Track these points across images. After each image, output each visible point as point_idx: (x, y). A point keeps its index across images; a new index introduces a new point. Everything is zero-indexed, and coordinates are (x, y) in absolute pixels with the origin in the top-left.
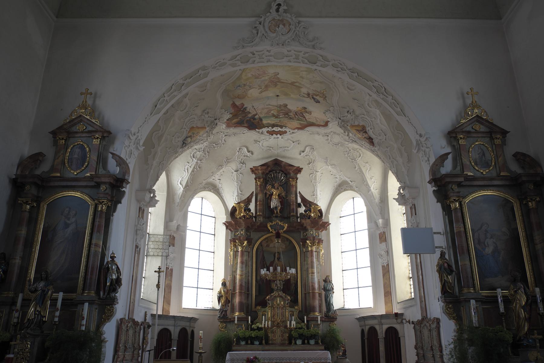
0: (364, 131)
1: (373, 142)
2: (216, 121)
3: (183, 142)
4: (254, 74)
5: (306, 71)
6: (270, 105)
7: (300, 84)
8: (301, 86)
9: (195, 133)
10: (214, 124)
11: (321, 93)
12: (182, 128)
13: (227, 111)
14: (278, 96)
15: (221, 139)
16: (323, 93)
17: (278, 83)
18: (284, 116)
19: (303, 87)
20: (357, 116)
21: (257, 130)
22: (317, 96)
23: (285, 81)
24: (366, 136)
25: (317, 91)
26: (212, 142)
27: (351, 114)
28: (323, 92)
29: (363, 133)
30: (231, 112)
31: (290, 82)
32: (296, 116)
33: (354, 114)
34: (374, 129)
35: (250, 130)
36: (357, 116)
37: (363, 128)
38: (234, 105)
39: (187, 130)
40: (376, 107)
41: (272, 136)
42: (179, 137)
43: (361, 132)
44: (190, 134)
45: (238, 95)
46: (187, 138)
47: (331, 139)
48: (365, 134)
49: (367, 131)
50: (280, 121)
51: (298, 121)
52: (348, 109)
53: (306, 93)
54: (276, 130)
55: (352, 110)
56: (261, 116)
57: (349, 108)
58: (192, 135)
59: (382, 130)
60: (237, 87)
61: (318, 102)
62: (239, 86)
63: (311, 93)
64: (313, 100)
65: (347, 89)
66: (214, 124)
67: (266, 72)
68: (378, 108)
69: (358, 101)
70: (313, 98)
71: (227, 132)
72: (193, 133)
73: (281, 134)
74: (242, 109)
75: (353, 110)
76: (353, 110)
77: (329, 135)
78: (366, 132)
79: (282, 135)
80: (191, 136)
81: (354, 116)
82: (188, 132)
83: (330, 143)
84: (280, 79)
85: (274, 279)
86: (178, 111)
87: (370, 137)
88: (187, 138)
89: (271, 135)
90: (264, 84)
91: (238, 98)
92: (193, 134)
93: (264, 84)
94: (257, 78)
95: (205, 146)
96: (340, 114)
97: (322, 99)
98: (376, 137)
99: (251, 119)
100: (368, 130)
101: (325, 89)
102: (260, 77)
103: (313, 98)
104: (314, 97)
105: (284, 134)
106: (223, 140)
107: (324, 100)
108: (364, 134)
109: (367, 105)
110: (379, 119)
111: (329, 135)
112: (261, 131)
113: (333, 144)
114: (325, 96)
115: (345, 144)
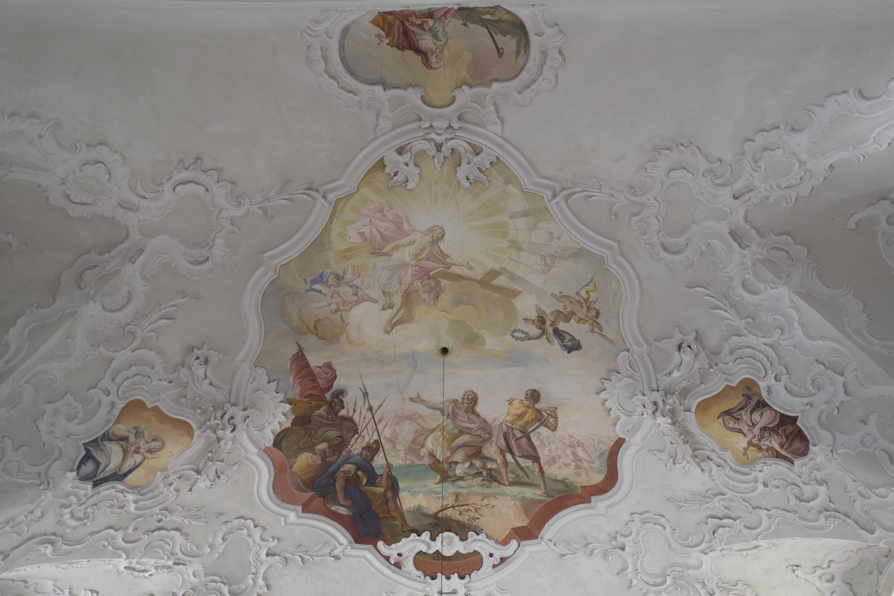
0: (754, 403)
1: (800, 431)
2: (231, 411)
3: (86, 449)
4: (366, 230)
5: (526, 214)
6: (422, 402)
7: (513, 277)
8: (516, 287)
9: (146, 434)
10: (222, 417)
11: (578, 301)
12: (96, 385)
13: (274, 385)
14: (445, 351)
15: (253, 570)
16: (586, 301)
17: (444, 282)
18: (467, 464)
19: (520, 292)
20: (716, 353)
21: (381, 544)
22: (567, 319)
23: (465, 272)
24: (764, 419)
25: (567, 297)
26: (220, 576)
27: (694, 346)
28: (588, 292)
29: (752, 412)
30: (291, 395)
31: (479, 274)
32: (509, 457)
33: (704, 349)
34: (788, 374)
35: (356, 542)
36: (716, 353)
37: (746, 392)
38: (300, 361)
39: (113, 404)
40: (773, 282)
41: (433, 582)
42: (75, 417)
43: (743, 412)
44: (121, 429)
45: (318, 321)
46: (110, 440)
47: (635, 564)
48: (761, 415)
49: (764, 395)
50: (457, 496)
51: (516, 490)
52: (678, 337)
53: (533, 315)
54: (448, 552)
55: (694, 335)
56: (396, 462)
57: (680, 332)
58: (132, 438)
59: (821, 360)
60: (314, 282)
61: (573, 346)
62: (320, 279)
63: (548, 311)
64: (556, 341)
65: (663, 254)
66: (222, 417)
67: (406, 227)
68: (784, 281)
69: (707, 289)
70: (558, 333)
71: (276, 535)
72: (135, 428)
73: (462, 573)
74: (328, 396)
75: (697, 332)
76: (697, 332)
77: (626, 541)
78: (762, 405)
79: (467, 576)
80: (125, 439)
81: (703, 355)
82: (117, 412)
83: (634, 582)
84: (448, 260)
85: (545, 441)
86: (91, 303)
87: (782, 415)
88: (106, 437)
89: (428, 578)
90: (401, 284)
91: (317, 334)
92: (136, 435)
93: (401, 284)
94: (377, 252)
95: (189, 585)
96: (655, 372)
97: (586, 327)
98: (806, 400)
99: (360, 473)
100: (769, 387)
101: (592, 280)
102: (385, 250)
103: (558, 333)
104: (562, 326)
105: (473, 575)
106: (260, 576)
107: (592, 332)
108: (756, 416)
109: (741, 291)
110: (796, 326)
111: (626, 541)
112: (392, 551)
113: (647, 587)
114: (594, 313)
115: (688, 568)
